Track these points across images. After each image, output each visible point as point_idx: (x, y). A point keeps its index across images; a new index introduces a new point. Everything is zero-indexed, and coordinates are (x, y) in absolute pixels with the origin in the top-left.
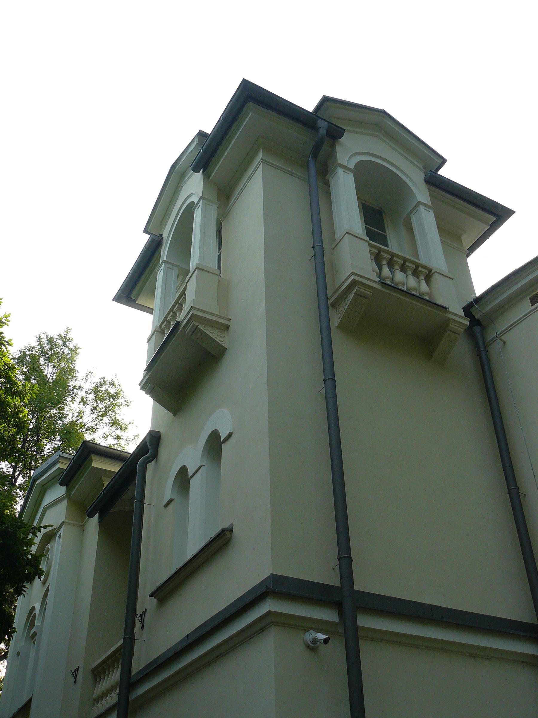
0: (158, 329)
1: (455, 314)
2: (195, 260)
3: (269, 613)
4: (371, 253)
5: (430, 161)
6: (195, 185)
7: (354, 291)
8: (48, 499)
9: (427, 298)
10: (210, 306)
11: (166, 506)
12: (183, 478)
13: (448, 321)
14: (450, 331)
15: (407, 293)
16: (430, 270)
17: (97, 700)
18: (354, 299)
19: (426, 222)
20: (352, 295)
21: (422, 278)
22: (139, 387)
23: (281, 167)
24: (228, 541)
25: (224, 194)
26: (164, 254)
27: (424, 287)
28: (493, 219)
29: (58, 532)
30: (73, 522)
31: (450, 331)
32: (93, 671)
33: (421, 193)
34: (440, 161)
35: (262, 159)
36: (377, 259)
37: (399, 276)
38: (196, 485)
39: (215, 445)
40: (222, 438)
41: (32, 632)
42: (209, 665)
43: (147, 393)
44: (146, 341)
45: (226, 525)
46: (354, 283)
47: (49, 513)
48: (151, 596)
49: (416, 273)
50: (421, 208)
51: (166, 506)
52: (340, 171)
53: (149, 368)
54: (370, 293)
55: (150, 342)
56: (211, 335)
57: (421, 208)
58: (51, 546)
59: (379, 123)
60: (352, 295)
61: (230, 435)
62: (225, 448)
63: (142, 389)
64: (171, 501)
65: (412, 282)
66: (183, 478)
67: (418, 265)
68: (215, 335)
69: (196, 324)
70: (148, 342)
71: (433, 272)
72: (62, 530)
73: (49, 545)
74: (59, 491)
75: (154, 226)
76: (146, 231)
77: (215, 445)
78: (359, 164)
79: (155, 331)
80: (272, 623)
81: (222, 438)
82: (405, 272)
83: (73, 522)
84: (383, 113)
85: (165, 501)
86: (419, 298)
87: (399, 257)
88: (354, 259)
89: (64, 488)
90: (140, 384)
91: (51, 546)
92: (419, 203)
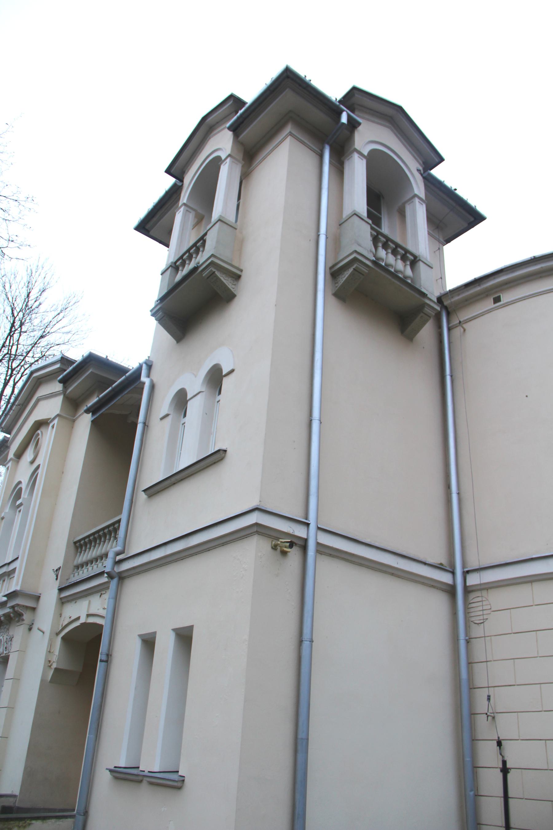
0: (173, 265)
1: (430, 300)
2: (218, 210)
3: (257, 524)
4: (371, 235)
5: (430, 157)
6: (223, 143)
7: (354, 267)
8: (43, 391)
9: (409, 281)
10: (225, 254)
11: (162, 419)
12: (181, 400)
13: (424, 305)
14: (425, 314)
15: (394, 275)
16: (415, 257)
17: (77, 567)
18: (352, 274)
19: (419, 214)
20: (351, 270)
21: (408, 263)
22: (150, 313)
23: (301, 140)
24: (222, 459)
25: (250, 155)
26: (184, 197)
27: (409, 272)
28: (472, 219)
29: (51, 422)
30: (67, 416)
31: (425, 314)
32: (75, 543)
33: (418, 187)
34: (437, 160)
35: (290, 132)
36: (375, 240)
37: (391, 259)
38: (195, 407)
39: (216, 378)
40: (224, 373)
41: (18, 502)
42: (321, 554)
43: (156, 320)
44: (160, 273)
45: (224, 448)
46: (355, 260)
47: (42, 404)
48: (144, 491)
49: (404, 258)
50: (417, 200)
51: (162, 419)
52: (356, 155)
53: (162, 299)
54: (365, 270)
55: (165, 274)
56: (224, 281)
57: (417, 200)
58: (42, 432)
59: (394, 116)
60: (351, 270)
61: (232, 371)
62: (225, 381)
63: (153, 315)
64: (167, 415)
65: (400, 265)
66: (181, 400)
67: (407, 251)
68: (227, 282)
69: (214, 270)
70: (161, 274)
71: (418, 259)
72: (56, 421)
73: (39, 432)
74: (59, 387)
75: (176, 169)
76: (168, 171)
77: (216, 378)
78: (372, 152)
79: (171, 266)
80: (258, 533)
81: (224, 373)
82: (386, 250)
83: (67, 416)
84: (400, 109)
85: (161, 416)
86: (403, 281)
87: (412, 254)
88: (360, 239)
89: (62, 385)
90: (151, 311)
91: (42, 432)
92: (416, 196)
